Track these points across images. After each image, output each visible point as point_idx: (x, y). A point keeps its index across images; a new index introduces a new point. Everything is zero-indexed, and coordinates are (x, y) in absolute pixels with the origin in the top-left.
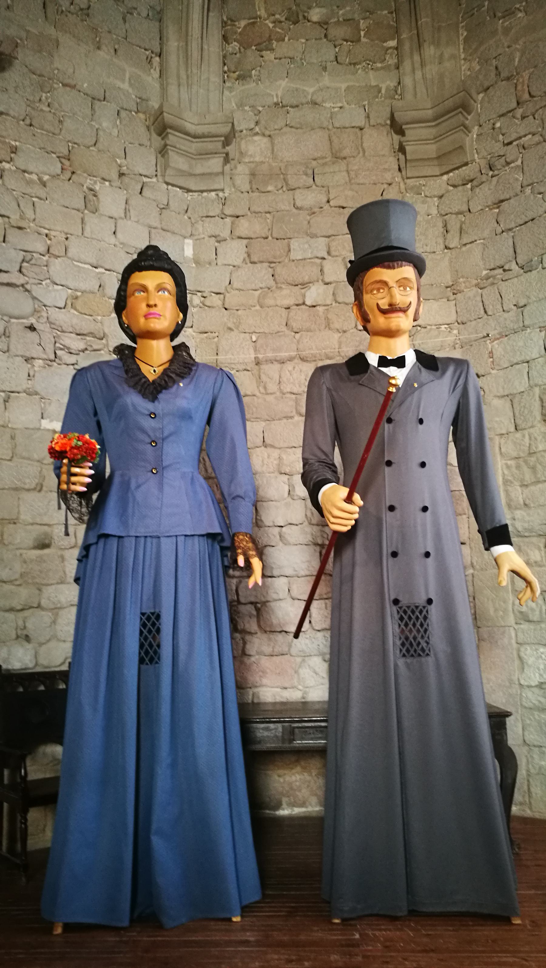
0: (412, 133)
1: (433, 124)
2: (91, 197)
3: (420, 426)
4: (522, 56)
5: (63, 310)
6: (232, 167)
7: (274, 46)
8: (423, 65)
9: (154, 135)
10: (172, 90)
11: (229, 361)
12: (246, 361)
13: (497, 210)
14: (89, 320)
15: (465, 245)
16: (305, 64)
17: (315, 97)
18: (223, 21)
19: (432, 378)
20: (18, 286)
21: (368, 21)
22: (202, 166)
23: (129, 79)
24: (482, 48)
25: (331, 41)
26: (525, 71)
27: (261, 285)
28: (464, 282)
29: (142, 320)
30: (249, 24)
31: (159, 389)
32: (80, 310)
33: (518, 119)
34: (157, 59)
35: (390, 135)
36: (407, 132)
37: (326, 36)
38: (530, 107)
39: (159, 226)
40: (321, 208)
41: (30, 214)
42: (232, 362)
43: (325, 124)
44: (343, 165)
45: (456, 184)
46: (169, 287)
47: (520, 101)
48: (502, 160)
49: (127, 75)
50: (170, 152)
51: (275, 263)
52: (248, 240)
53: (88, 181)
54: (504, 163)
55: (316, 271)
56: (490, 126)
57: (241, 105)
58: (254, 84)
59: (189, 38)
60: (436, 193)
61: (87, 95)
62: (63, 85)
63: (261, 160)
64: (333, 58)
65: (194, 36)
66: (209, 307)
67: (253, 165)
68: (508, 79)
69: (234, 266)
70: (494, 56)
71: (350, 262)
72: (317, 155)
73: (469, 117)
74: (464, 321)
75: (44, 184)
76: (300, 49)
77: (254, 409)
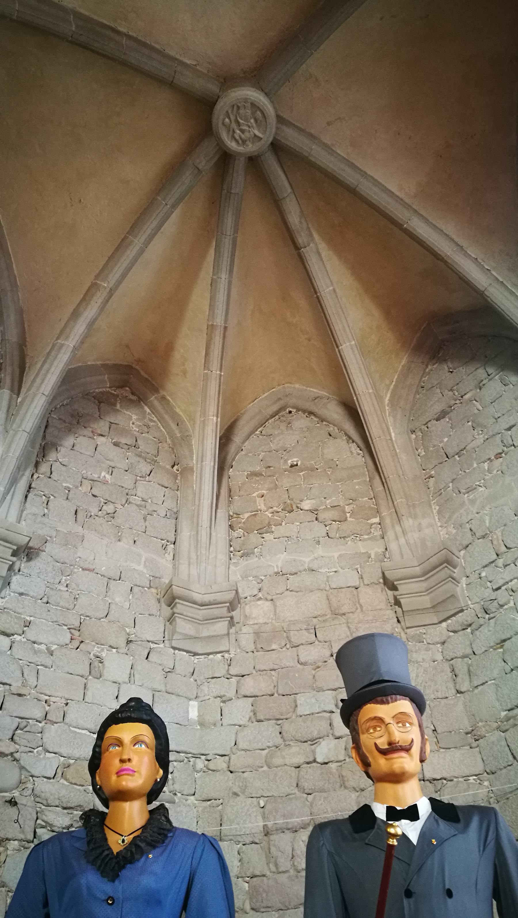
0: (403, 588)
1: (423, 579)
2: (96, 663)
3: (449, 901)
4: (491, 519)
5: (52, 780)
6: (238, 629)
7: (273, 529)
8: (404, 533)
9: (164, 606)
10: (183, 568)
11: (234, 832)
12: (253, 831)
13: (501, 650)
14: (79, 790)
15: (477, 687)
16: (300, 540)
17: (311, 565)
18: (229, 516)
19: (453, 832)
20: (7, 755)
21: (352, 506)
22: (208, 630)
23: (145, 562)
24: (455, 516)
25: (321, 522)
26: (496, 529)
27: (268, 744)
28: (484, 727)
29: (114, 778)
30: (251, 515)
31: (122, 863)
32: (71, 780)
33: (501, 568)
34: (172, 545)
35: (384, 592)
36: (399, 587)
37: (317, 519)
38: (509, 557)
39: (164, 689)
40: (326, 662)
41: (32, 681)
42: (238, 833)
43: (323, 586)
44: (343, 619)
45: (457, 630)
46: (146, 739)
47: (499, 553)
48: (495, 603)
49: (143, 559)
50: (177, 619)
51: (282, 719)
52: (254, 698)
53: (96, 649)
54: (498, 606)
55: (325, 725)
56: (477, 576)
57: (245, 577)
58: (257, 559)
59: (200, 528)
60: (438, 640)
61: (104, 576)
62: (83, 569)
63: (264, 622)
64: (325, 534)
65: (203, 526)
66: (214, 771)
67: (256, 627)
68: (483, 537)
69: (240, 726)
70: (467, 521)
71: (342, 700)
72: (316, 613)
73: (455, 571)
74: (494, 770)
75: (51, 653)
76: (295, 530)
77: (264, 895)
